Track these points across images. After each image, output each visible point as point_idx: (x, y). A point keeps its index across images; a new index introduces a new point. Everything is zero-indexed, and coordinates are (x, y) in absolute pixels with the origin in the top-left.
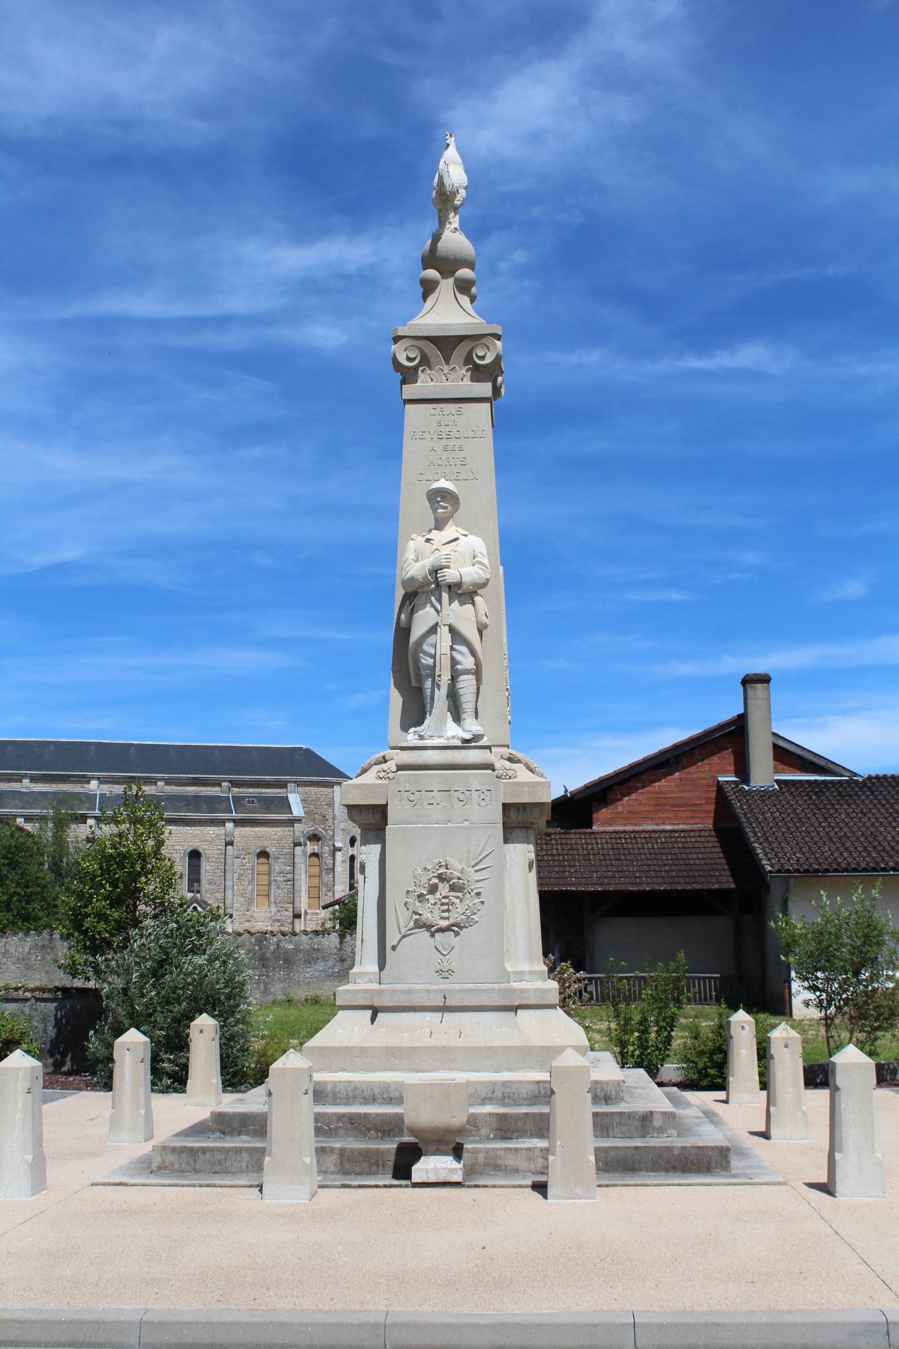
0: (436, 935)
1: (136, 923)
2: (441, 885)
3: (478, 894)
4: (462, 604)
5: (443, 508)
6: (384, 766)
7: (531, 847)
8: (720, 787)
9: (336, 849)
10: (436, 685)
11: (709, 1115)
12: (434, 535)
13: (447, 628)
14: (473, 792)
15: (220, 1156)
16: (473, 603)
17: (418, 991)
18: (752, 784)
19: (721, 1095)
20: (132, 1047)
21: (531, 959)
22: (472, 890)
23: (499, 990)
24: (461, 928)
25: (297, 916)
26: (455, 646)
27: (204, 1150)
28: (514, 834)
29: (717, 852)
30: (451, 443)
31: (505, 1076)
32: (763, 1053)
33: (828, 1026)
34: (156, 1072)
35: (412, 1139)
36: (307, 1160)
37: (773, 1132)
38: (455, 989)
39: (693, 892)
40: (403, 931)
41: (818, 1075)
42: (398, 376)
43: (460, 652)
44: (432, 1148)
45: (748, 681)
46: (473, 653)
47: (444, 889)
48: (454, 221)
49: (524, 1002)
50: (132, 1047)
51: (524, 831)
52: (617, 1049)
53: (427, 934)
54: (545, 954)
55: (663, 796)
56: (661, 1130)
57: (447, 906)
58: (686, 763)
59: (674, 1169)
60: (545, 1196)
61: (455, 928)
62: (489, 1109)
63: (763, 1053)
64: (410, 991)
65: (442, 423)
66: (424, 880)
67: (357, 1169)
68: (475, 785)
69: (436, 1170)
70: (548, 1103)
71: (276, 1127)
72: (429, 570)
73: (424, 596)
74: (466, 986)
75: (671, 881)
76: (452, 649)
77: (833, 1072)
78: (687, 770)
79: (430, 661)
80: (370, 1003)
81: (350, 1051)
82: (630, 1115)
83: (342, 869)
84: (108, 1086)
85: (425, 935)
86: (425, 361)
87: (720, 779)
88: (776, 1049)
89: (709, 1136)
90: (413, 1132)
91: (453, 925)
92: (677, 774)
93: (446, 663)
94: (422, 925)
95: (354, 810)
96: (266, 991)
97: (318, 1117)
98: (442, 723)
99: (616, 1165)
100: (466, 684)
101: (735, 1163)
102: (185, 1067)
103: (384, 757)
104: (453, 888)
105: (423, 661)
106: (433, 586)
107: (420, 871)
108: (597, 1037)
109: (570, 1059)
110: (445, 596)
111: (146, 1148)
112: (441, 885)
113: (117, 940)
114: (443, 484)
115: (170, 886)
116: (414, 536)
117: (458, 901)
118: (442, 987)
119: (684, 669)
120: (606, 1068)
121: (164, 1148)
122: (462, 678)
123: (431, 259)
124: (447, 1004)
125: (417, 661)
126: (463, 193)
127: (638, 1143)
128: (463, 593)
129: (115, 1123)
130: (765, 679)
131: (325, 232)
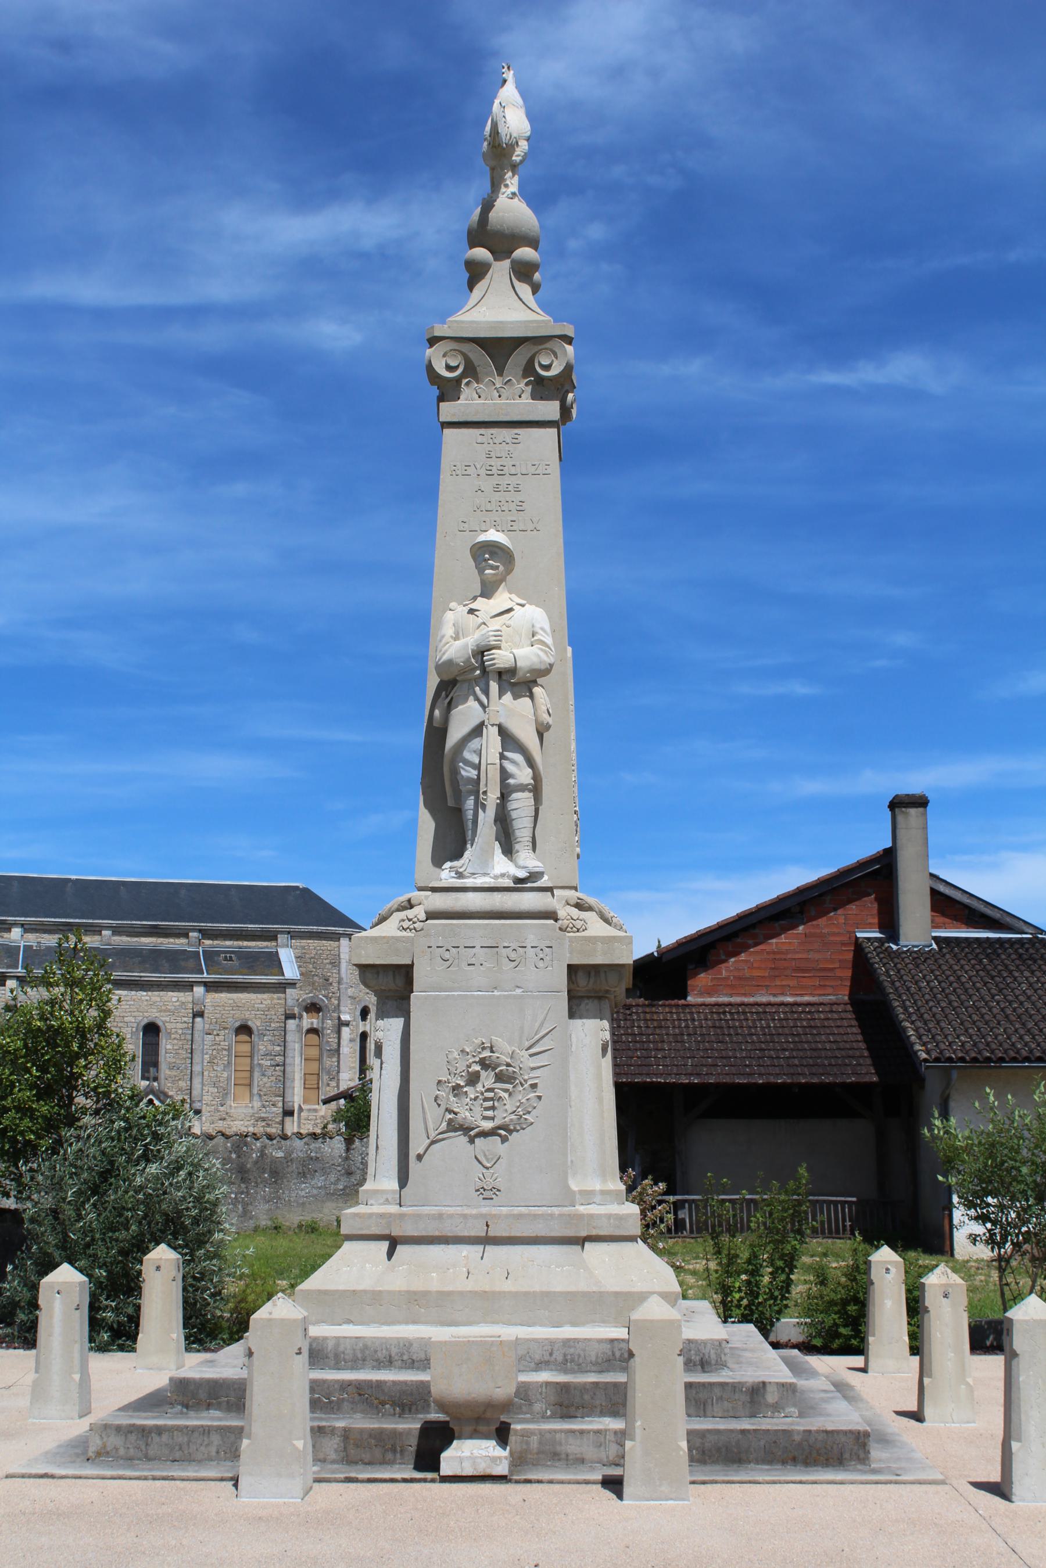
0: (477, 1140)
1: (71, 1121)
2: (483, 1074)
3: (534, 1086)
4: (516, 697)
5: (492, 567)
6: (410, 913)
7: (606, 1024)
8: (858, 946)
9: (342, 1024)
10: (480, 805)
11: (841, 1388)
12: (480, 603)
13: (496, 729)
14: (529, 949)
15: (181, 1439)
16: (531, 696)
17: (451, 1216)
18: (902, 943)
19: (858, 1361)
20: (64, 1288)
21: (604, 1175)
22: (526, 1081)
23: (561, 1215)
24: (510, 1132)
25: (288, 1113)
26: (506, 753)
27: (159, 1430)
28: (583, 1006)
29: (853, 1033)
30: (504, 481)
31: (568, 1332)
32: (915, 1307)
33: (1002, 1270)
34: (95, 1324)
35: (441, 1417)
36: (300, 1444)
37: (928, 1412)
38: (502, 1214)
39: (822, 1086)
40: (433, 1134)
41: (988, 1336)
42: (435, 391)
43: (513, 762)
44: (468, 1429)
45: (898, 804)
46: (530, 762)
47: (487, 1079)
48: (512, 183)
49: (594, 1233)
50: (64, 1288)
51: (596, 1001)
52: (718, 1297)
53: (464, 1140)
54: (623, 1168)
55: (783, 957)
56: (776, 1408)
57: (492, 1102)
58: (813, 913)
59: (794, 1460)
60: (620, 1496)
61: (502, 1132)
62: (545, 1376)
63: (915, 1307)
64: (440, 1216)
65: (492, 454)
66: (461, 1066)
67: (367, 1457)
68: (531, 940)
69: (473, 1459)
70: (625, 1369)
71: (258, 1399)
72: (473, 651)
73: (466, 685)
74: (516, 1210)
75: (792, 1071)
76: (502, 757)
77: (1010, 1332)
78: (814, 923)
79: (473, 773)
80: (387, 1232)
81: (364, 1294)
82: (735, 1387)
83: (349, 1050)
84: (30, 1342)
85: (460, 1140)
86: (471, 371)
87: (859, 935)
88: (932, 1300)
89: (841, 1417)
90: (442, 1406)
91: (499, 1128)
92: (801, 928)
93: (494, 775)
94: (457, 1127)
95: (368, 972)
96: (245, 1214)
97: (315, 1386)
98: (486, 858)
99: (718, 1454)
100: (521, 804)
101: (877, 1453)
102: (135, 1320)
103: (409, 901)
104: (500, 1078)
105: (463, 773)
106: (478, 672)
107: (456, 1054)
108: (691, 1280)
109: (655, 1310)
110: (494, 686)
111: (81, 1427)
112: (483, 1074)
113: (46, 1142)
114: (493, 535)
115: (119, 1070)
116: (453, 605)
117: (506, 1095)
118: (484, 1210)
119: (812, 787)
120: (704, 1323)
121: (106, 1427)
122: (515, 796)
123: (481, 234)
124: (490, 1234)
125: (455, 772)
126: (524, 145)
127: (746, 1424)
128: (519, 682)
129: (38, 1392)
130: (920, 802)
131: (334, 195)
